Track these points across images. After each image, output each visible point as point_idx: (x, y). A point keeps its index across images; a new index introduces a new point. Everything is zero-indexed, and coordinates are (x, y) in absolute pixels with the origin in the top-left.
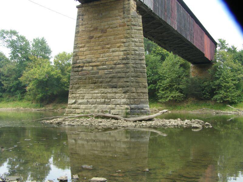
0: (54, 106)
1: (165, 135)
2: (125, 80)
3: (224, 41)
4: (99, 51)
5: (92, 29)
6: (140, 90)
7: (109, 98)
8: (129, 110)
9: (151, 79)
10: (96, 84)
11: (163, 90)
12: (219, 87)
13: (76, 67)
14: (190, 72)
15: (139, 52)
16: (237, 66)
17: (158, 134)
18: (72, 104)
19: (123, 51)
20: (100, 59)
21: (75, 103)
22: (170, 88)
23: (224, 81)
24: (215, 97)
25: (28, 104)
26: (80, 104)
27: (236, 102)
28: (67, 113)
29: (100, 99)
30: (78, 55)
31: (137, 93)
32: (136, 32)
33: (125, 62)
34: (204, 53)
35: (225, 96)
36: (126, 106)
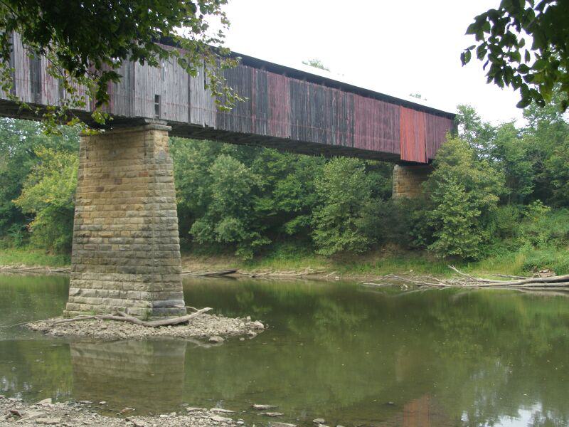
2: (146, 262)
5: (101, 175)
6: (168, 278)
7: (125, 288)
8: (151, 309)
9: (301, 203)
10: (107, 266)
11: (325, 229)
12: (440, 225)
13: (80, 236)
14: (394, 183)
18: (75, 295)
19: (143, 216)
21: (79, 294)
22: (338, 224)
25: (38, 257)
26: (86, 295)
31: (164, 282)
32: (164, 186)
36: (147, 303)
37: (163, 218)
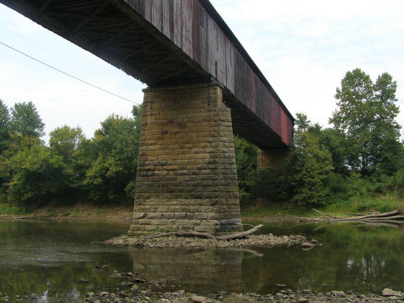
0: (49, 211)
1: (261, 255)
2: (213, 188)
3: (305, 117)
4: (176, 151)
5: (166, 121)
6: (231, 201)
12: (301, 183)
13: (144, 170)
15: (229, 154)
16: (324, 153)
17: (253, 254)
19: (209, 153)
20: (179, 161)
21: (143, 217)
23: (308, 175)
24: (296, 197)
26: (152, 218)
27: (323, 204)
28: (132, 231)
29: (179, 212)
30: (147, 154)
31: (228, 205)
33: (213, 167)
34: (282, 137)
35: (309, 196)
36: (215, 221)
37: (226, 154)
